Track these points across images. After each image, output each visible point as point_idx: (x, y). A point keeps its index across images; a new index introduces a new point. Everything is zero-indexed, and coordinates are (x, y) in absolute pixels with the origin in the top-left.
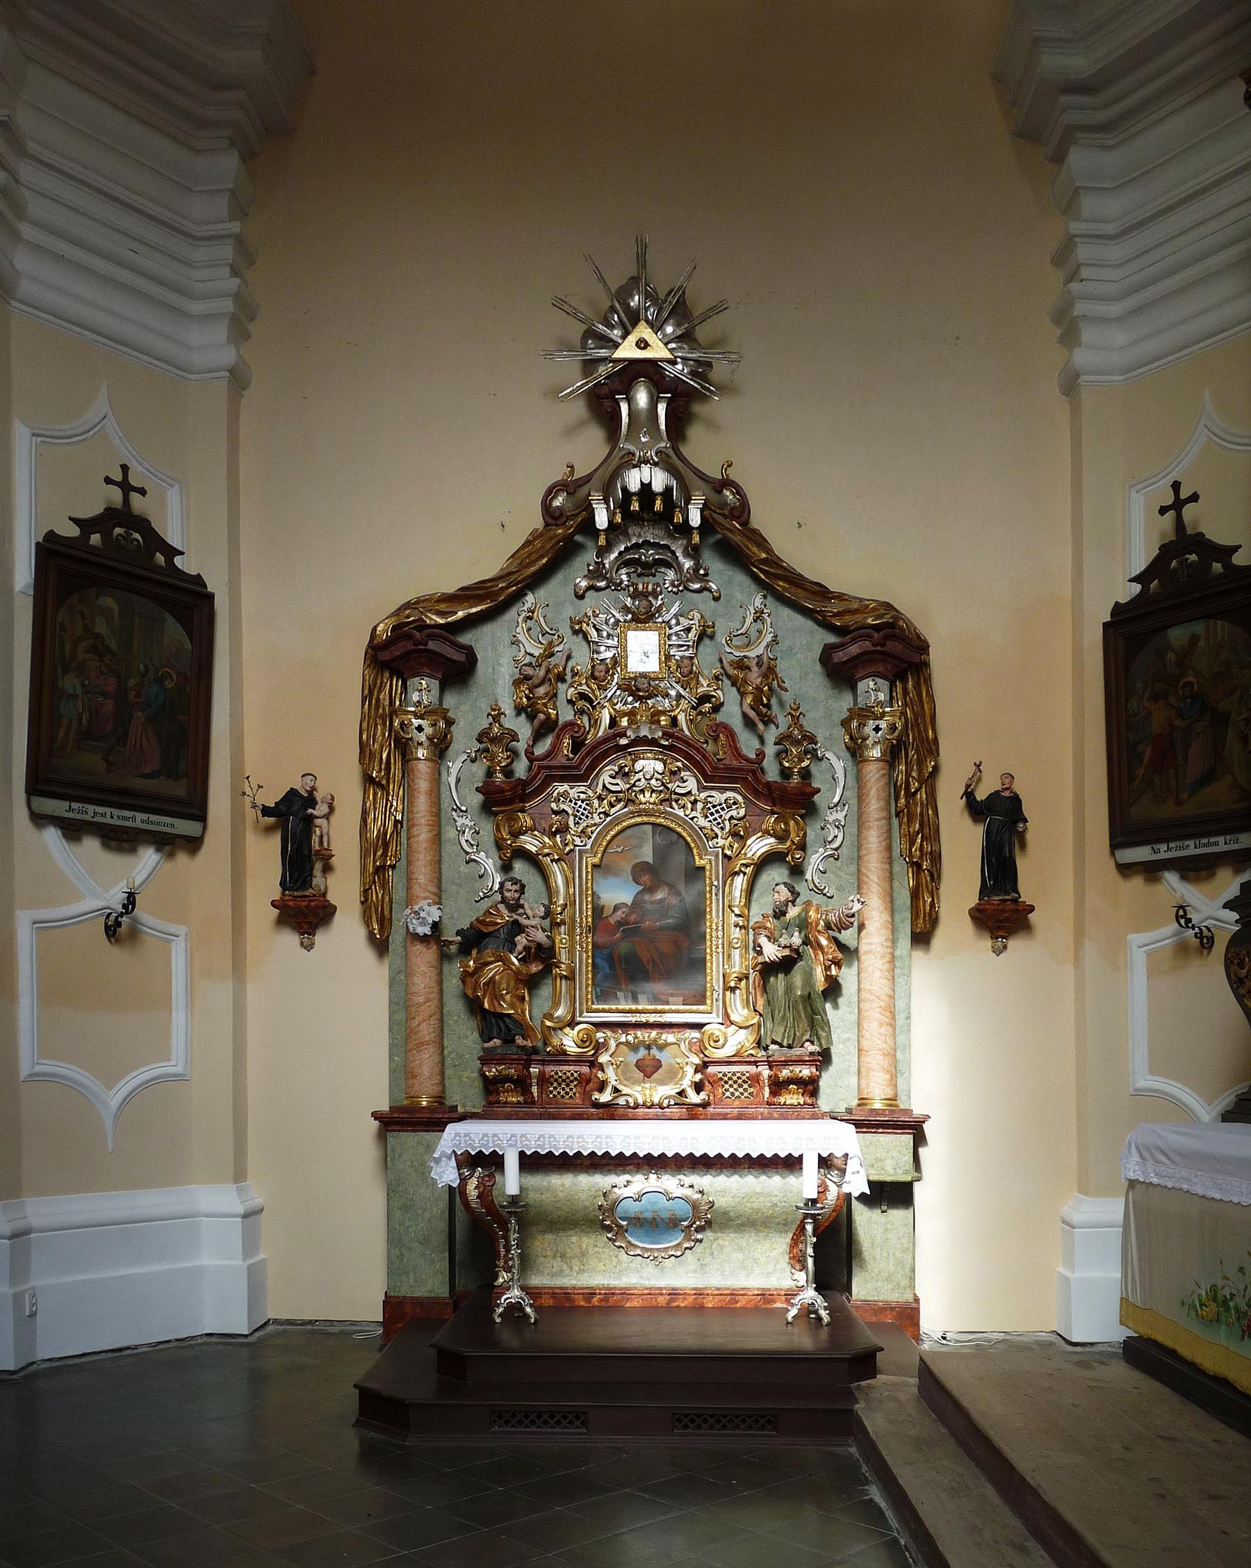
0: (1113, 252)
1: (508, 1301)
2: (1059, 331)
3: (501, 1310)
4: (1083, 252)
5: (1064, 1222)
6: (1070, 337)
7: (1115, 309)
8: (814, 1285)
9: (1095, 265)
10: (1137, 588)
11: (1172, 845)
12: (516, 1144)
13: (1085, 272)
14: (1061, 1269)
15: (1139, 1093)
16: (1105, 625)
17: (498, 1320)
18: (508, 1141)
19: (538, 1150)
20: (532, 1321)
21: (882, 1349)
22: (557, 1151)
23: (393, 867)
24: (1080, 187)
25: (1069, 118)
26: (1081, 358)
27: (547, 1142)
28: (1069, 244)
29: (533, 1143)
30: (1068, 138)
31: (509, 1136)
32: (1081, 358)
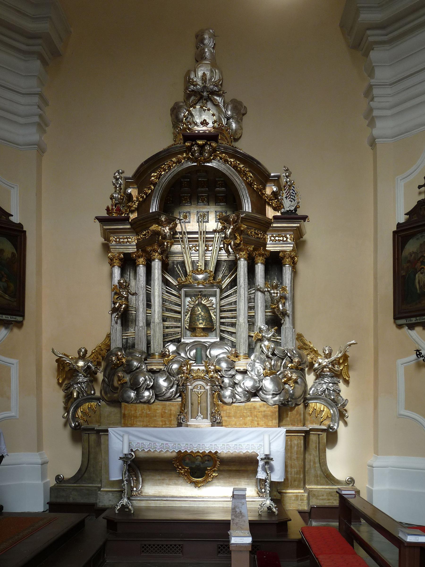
0: (388, 91)
1: (121, 504)
2: (367, 122)
3: (119, 508)
4: (375, 91)
5: (369, 466)
6: (372, 123)
7: (389, 113)
8: (270, 498)
9: (379, 97)
10: (408, 216)
11: (417, 318)
12: (237, 448)
13: (376, 99)
14: (367, 485)
15: (401, 416)
16: (394, 232)
17: (117, 512)
18: (245, 447)
19: (217, 451)
20: (132, 512)
21: (291, 520)
22: (213, 451)
23: (220, 249)
24: (375, 66)
25: (371, 39)
26: (375, 132)
27: (226, 447)
28: (370, 88)
29: (257, 448)
30: (370, 48)
31: (160, 444)
32: (375, 132)
